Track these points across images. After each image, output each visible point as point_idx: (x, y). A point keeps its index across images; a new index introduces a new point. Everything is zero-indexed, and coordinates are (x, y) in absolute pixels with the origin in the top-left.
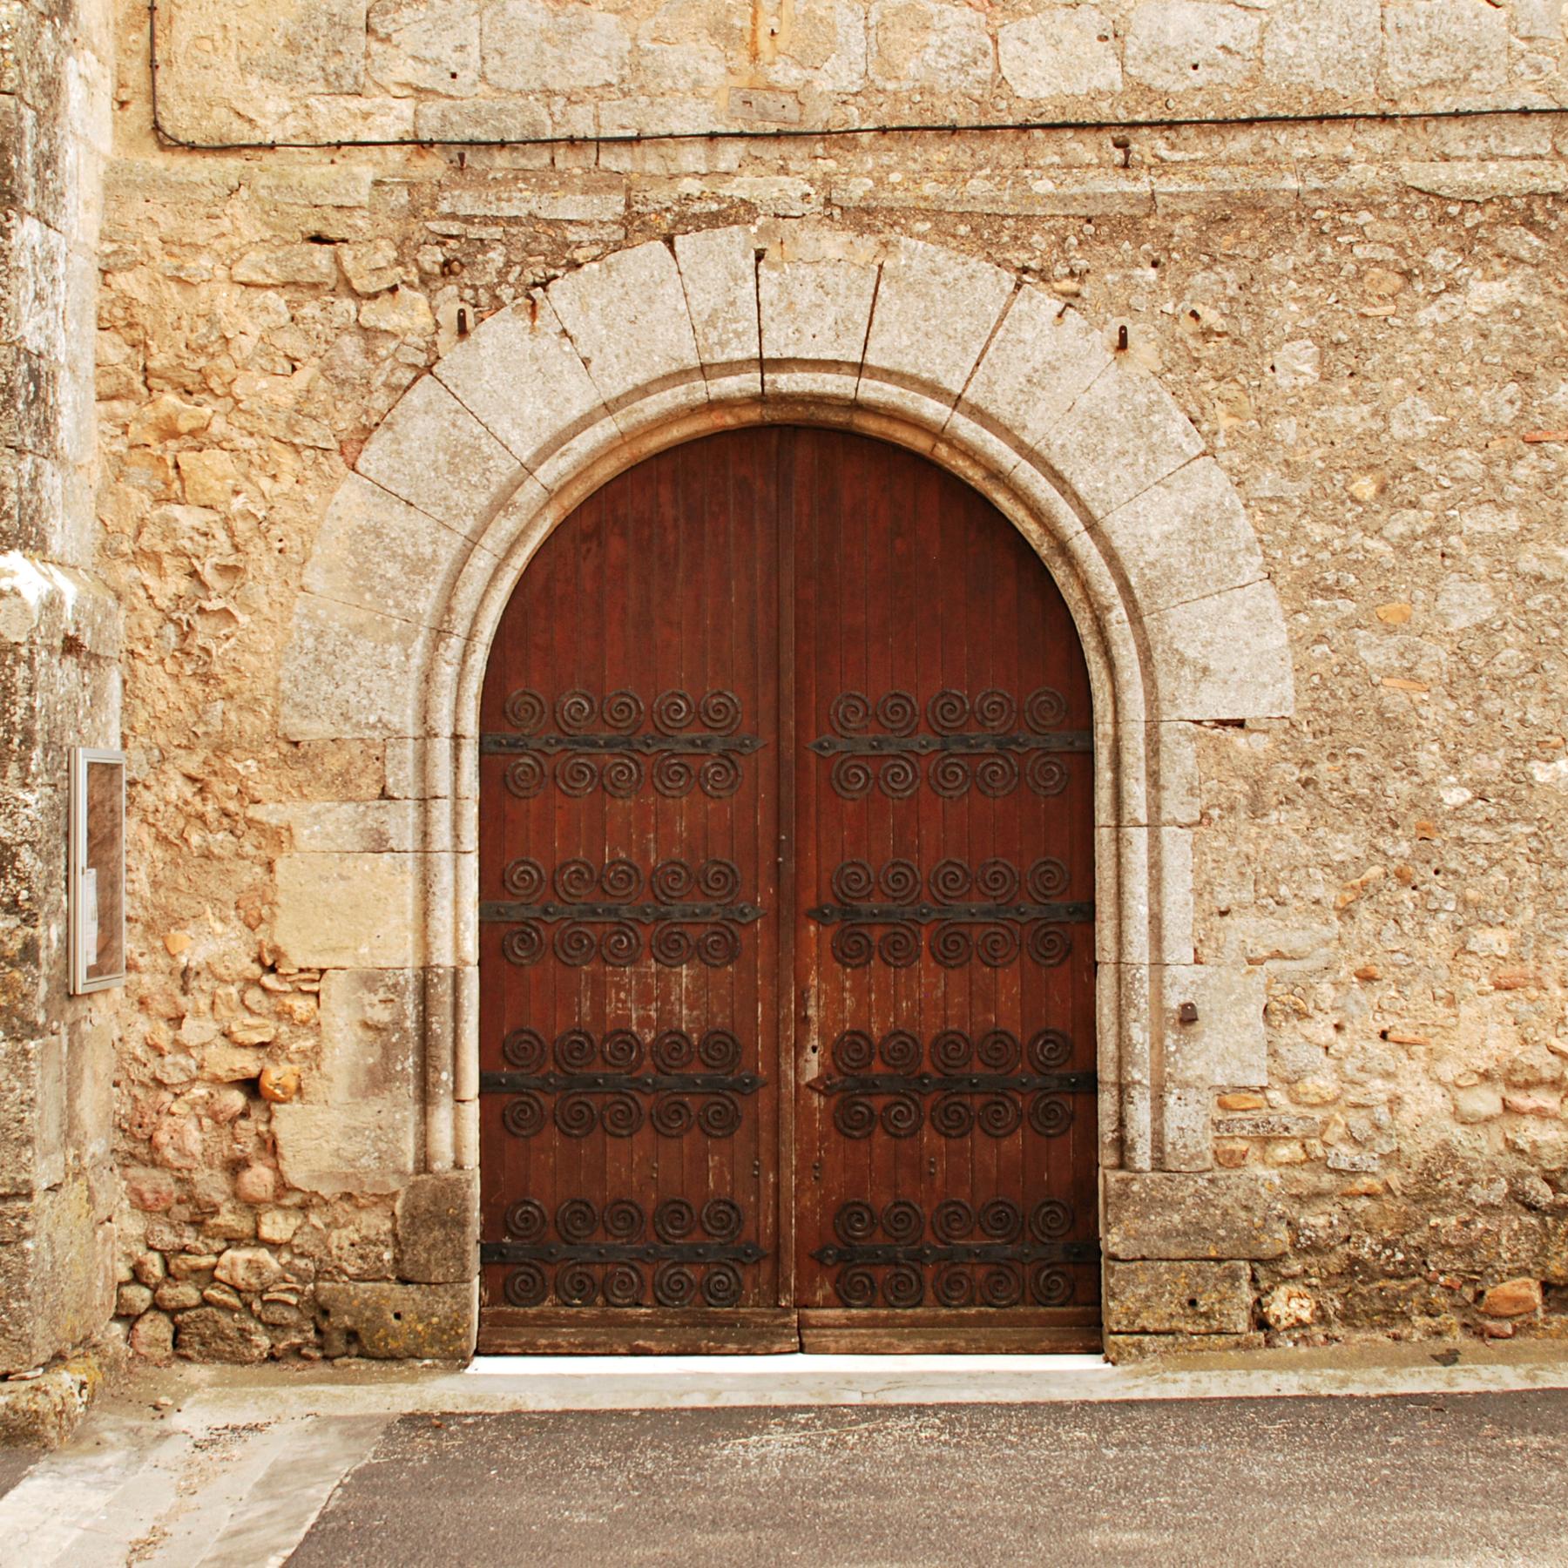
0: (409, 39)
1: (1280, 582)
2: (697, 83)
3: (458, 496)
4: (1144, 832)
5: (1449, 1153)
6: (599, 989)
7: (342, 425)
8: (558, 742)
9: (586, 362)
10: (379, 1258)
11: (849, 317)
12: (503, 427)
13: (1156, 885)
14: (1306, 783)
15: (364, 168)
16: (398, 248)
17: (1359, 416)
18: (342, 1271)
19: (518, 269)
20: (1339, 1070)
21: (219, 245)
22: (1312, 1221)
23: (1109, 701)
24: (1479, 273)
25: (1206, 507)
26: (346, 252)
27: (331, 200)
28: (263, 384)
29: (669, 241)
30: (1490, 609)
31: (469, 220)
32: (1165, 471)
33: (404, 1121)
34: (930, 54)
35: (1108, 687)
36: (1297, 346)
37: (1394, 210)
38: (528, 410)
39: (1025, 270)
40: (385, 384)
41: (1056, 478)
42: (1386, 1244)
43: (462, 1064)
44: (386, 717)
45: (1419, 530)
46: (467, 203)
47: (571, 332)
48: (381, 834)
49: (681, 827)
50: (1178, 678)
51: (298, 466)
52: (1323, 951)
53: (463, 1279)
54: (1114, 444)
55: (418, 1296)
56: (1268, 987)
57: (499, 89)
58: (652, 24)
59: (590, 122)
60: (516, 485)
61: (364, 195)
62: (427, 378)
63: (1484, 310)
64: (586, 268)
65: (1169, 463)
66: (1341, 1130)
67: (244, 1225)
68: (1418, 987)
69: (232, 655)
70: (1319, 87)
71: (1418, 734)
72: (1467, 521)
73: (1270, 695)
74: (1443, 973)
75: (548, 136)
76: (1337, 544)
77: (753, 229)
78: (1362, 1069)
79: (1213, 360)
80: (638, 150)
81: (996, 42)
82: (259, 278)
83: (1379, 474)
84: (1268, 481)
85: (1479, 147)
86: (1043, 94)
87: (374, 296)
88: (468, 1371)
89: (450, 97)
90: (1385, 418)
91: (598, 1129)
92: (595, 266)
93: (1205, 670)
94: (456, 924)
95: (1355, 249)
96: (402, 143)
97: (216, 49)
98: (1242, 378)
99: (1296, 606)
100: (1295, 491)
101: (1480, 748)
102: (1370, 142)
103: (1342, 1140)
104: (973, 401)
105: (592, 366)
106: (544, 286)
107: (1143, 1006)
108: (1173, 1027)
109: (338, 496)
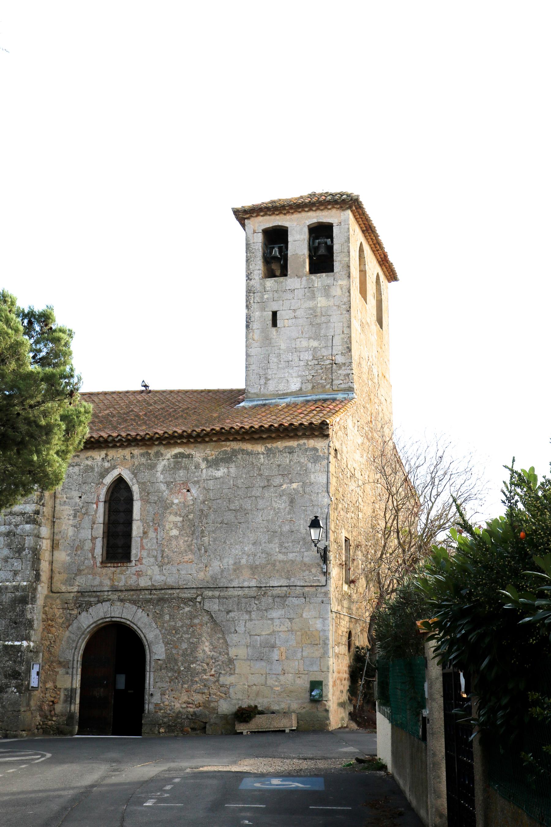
0: (78, 580)
12: (83, 625)
15: (72, 595)
60: (85, 631)
73: (163, 656)
79: (158, 617)
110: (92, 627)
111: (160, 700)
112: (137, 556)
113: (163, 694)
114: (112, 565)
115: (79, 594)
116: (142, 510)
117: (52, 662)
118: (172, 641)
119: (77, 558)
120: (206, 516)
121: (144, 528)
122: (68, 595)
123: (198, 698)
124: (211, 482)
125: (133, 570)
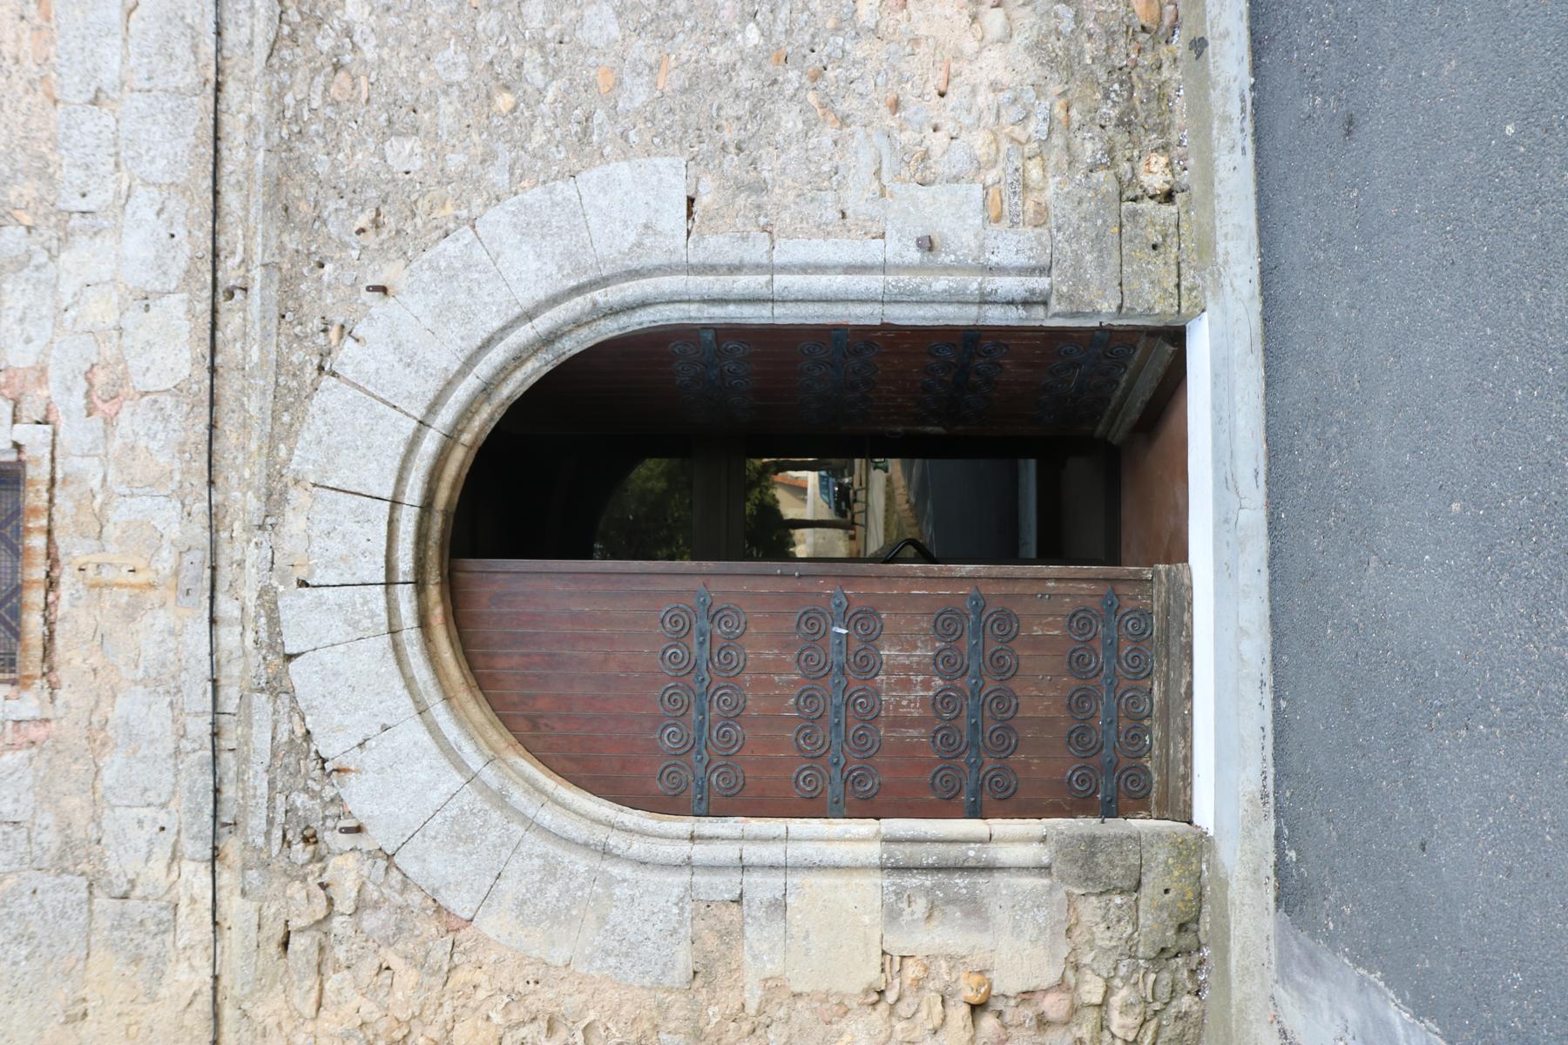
0: (133, 866)
1: (578, 168)
2: (172, 632)
3: (492, 837)
4: (776, 277)
5: (1036, 47)
6: (899, 722)
7: (434, 931)
8: (699, 753)
9: (385, 728)
10: (1120, 907)
11: (353, 511)
12: (436, 798)
13: (820, 269)
14: (740, 149)
15: (234, 908)
16: (293, 879)
17: (448, 106)
18: (1130, 937)
19: (310, 782)
20: (969, 129)
21: (287, 1028)
22: (1089, 153)
23: (671, 306)
24: (338, 13)
25: (515, 225)
26: (293, 925)
27: (253, 934)
28: (399, 995)
29: (290, 658)
30: (605, 7)
31: (270, 822)
32: (485, 257)
33: (1008, 886)
34: (154, 446)
35: (660, 307)
36: (389, 153)
37: (284, 76)
38: (423, 777)
39: (321, 368)
40: (402, 893)
41: (488, 344)
42: (1106, 97)
43: (961, 837)
44: (674, 899)
45: (541, 60)
46: (257, 822)
47: (360, 740)
48: (771, 905)
49: (769, 654)
50: (652, 248)
51: (467, 967)
52: (875, 139)
53: (1136, 839)
54: (462, 298)
55: (1152, 875)
56: (904, 181)
57: (174, 793)
58: (124, 669)
59: (200, 720)
60: (485, 788)
61: (251, 906)
62: (396, 859)
63: (368, 9)
64: (309, 727)
65: (479, 254)
66: (1017, 129)
67: (1092, 1015)
68: (903, 66)
69: (621, 1025)
70: (193, 140)
71: (703, 63)
72: (534, 24)
73: (668, 177)
74: (893, 47)
75: (209, 753)
76: (549, 123)
77: (281, 589)
78: (969, 111)
79: (394, 217)
80: (223, 681)
81: (147, 393)
82: (314, 995)
83: (495, 91)
84: (497, 176)
85: (244, 17)
86: (188, 355)
87: (330, 901)
88: (1211, 833)
89: (179, 832)
90: (450, 85)
91: (1011, 722)
92: (308, 719)
93: (646, 226)
94: (846, 840)
95: (314, 105)
96: (214, 871)
97: (137, 1023)
98: (414, 197)
99: (597, 156)
100: (505, 155)
101: (714, 16)
102: (237, 100)
103: (1025, 128)
104: (424, 411)
105: (389, 723)
106: (324, 761)
107: (918, 280)
108: (936, 256)
109: (492, 935)
110: (451, 731)
111: (961, 189)
113: (922, 169)
114: (35, 597)
118: (568, 109)
125: (75, 431)
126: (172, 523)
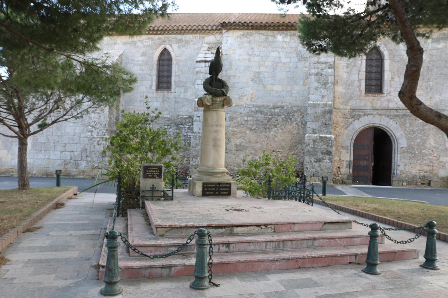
15: (347, 110)
79: (403, 125)
112: (387, 91)
113: (405, 165)
114: (372, 95)
115: (352, 110)
116: (390, 65)
117: (338, 146)
119: (349, 90)
120: (431, 70)
121: (392, 75)
122: (344, 111)
123: (426, 168)
124: (434, 51)
125: (386, 98)
126: (378, 106)
